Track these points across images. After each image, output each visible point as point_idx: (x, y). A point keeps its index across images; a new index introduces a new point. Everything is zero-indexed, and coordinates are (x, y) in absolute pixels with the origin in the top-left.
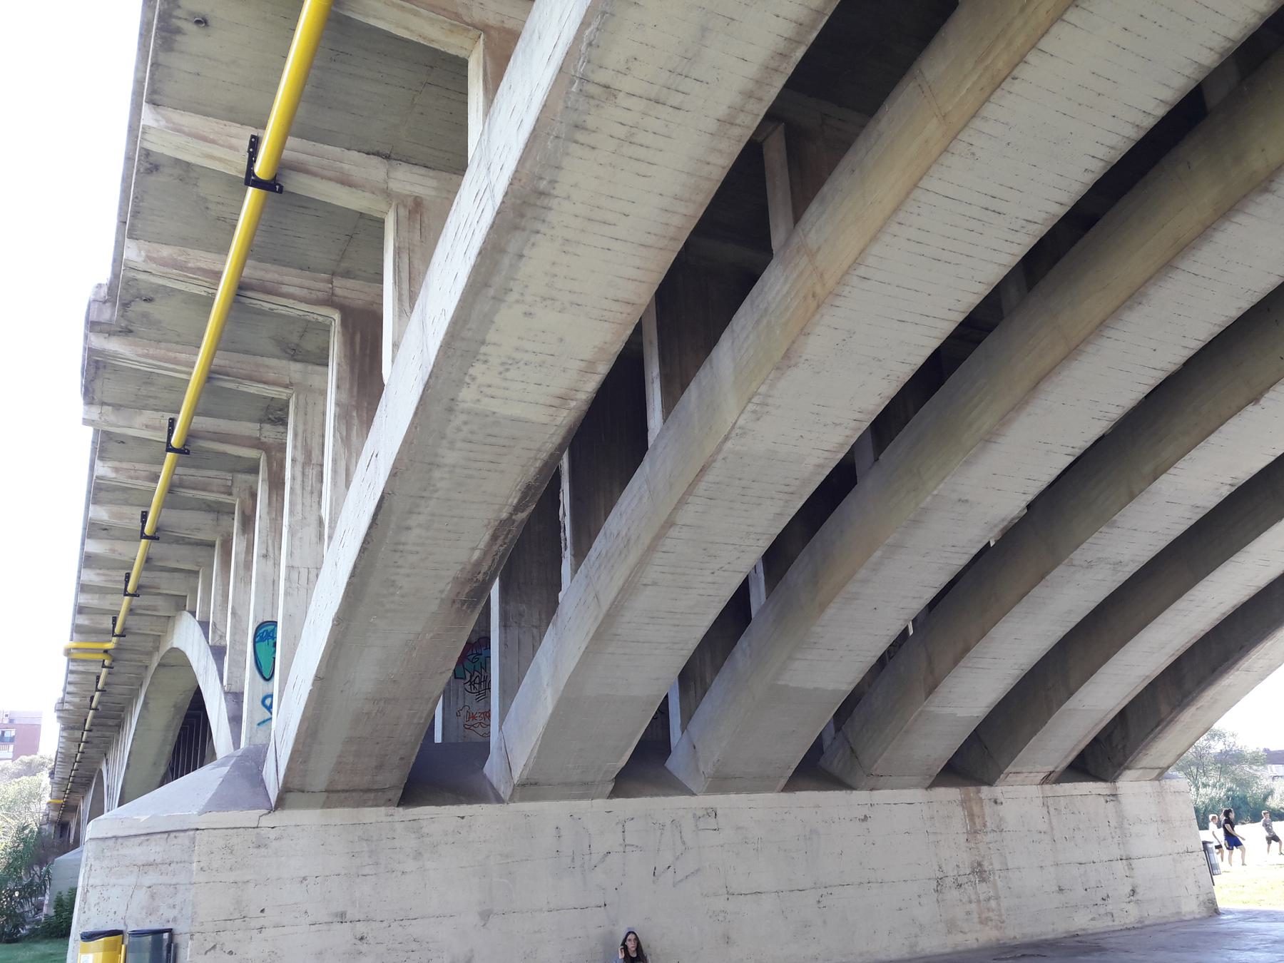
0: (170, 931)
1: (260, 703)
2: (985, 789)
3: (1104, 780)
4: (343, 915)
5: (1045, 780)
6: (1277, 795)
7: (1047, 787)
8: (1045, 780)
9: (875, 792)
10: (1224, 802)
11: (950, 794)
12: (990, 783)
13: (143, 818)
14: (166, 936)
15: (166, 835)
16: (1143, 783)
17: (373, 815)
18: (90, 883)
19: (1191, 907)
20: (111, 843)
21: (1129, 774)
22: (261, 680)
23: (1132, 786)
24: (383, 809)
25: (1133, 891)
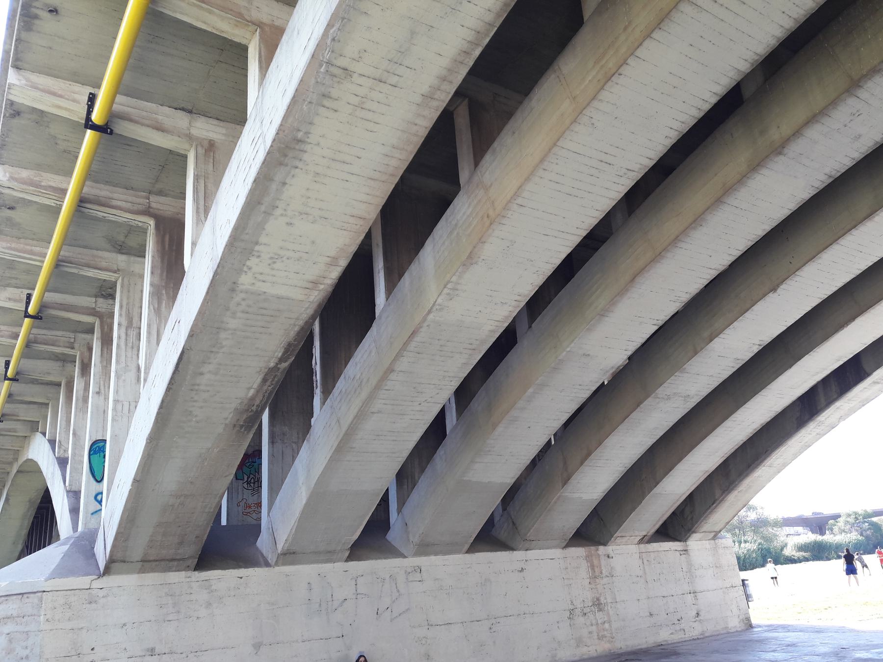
2: (601, 548)
5: (641, 541)
7: (642, 546)
8: (641, 541)
11: (579, 552)
15: (21, 596)
19: (734, 623)
21: (695, 536)
22: (95, 482)
23: (697, 544)
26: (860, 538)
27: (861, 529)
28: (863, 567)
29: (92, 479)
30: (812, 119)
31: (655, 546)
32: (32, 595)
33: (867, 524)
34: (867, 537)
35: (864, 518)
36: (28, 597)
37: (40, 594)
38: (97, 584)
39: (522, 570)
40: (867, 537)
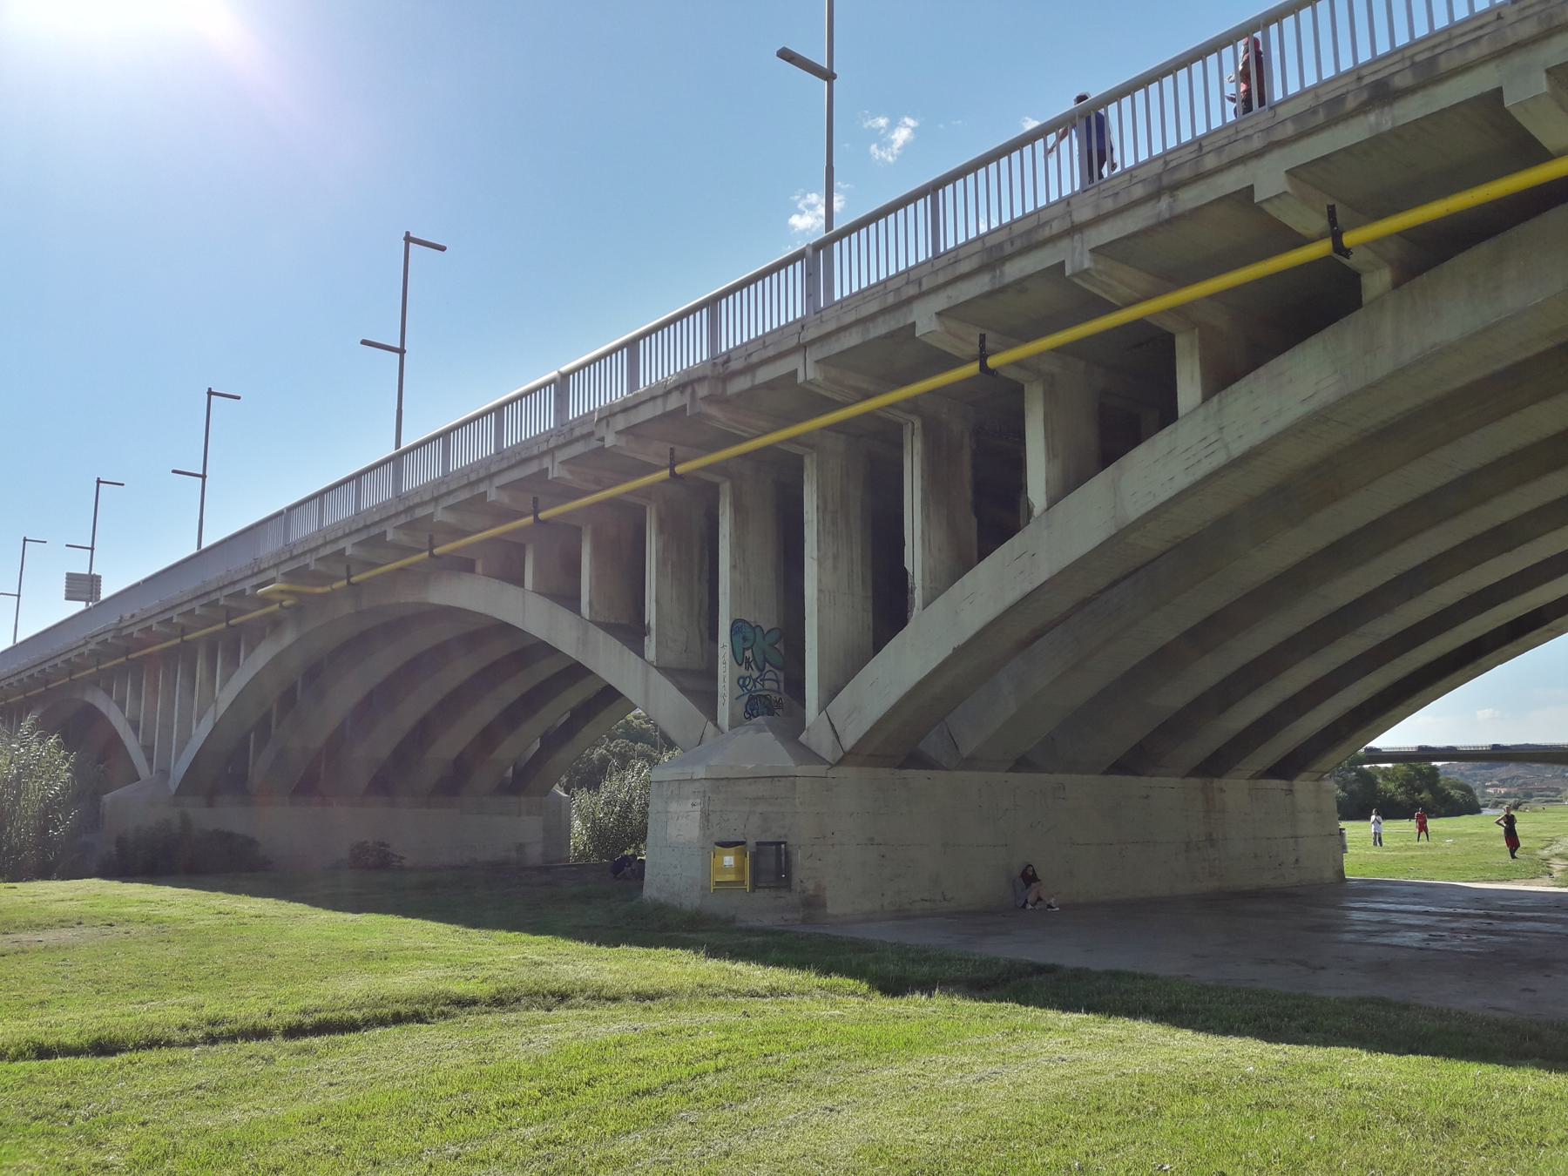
0: (785, 843)
1: (736, 683)
2: (1216, 780)
3: (1286, 779)
4: (872, 839)
5: (1251, 778)
6: (919, 325)
7: (1251, 781)
8: (1251, 778)
9: (1154, 779)
10: (1222, 1050)
11: (1195, 782)
12: (1219, 776)
13: (750, 767)
14: (783, 846)
15: (770, 779)
16: (1308, 782)
17: (884, 773)
18: (711, 808)
19: (1329, 875)
20: (724, 782)
21: (1305, 775)
22: (736, 665)
23: (1303, 785)
24: (887, 769)
25: (1297, 860)
26: (1342, 794)
27: (1344, 779)
28: (1420, 831)
29: (735, 662)
30: (1474, 61)
31: (1264, 783)
32: (784, 779)
33: (1354, 774)
34: (1351, 793)
35: (1350, 764)
36: (779, 781)
37: (792, 778)
38: (831, 774)
39: (1147, 797)
40: (1351, 793)
